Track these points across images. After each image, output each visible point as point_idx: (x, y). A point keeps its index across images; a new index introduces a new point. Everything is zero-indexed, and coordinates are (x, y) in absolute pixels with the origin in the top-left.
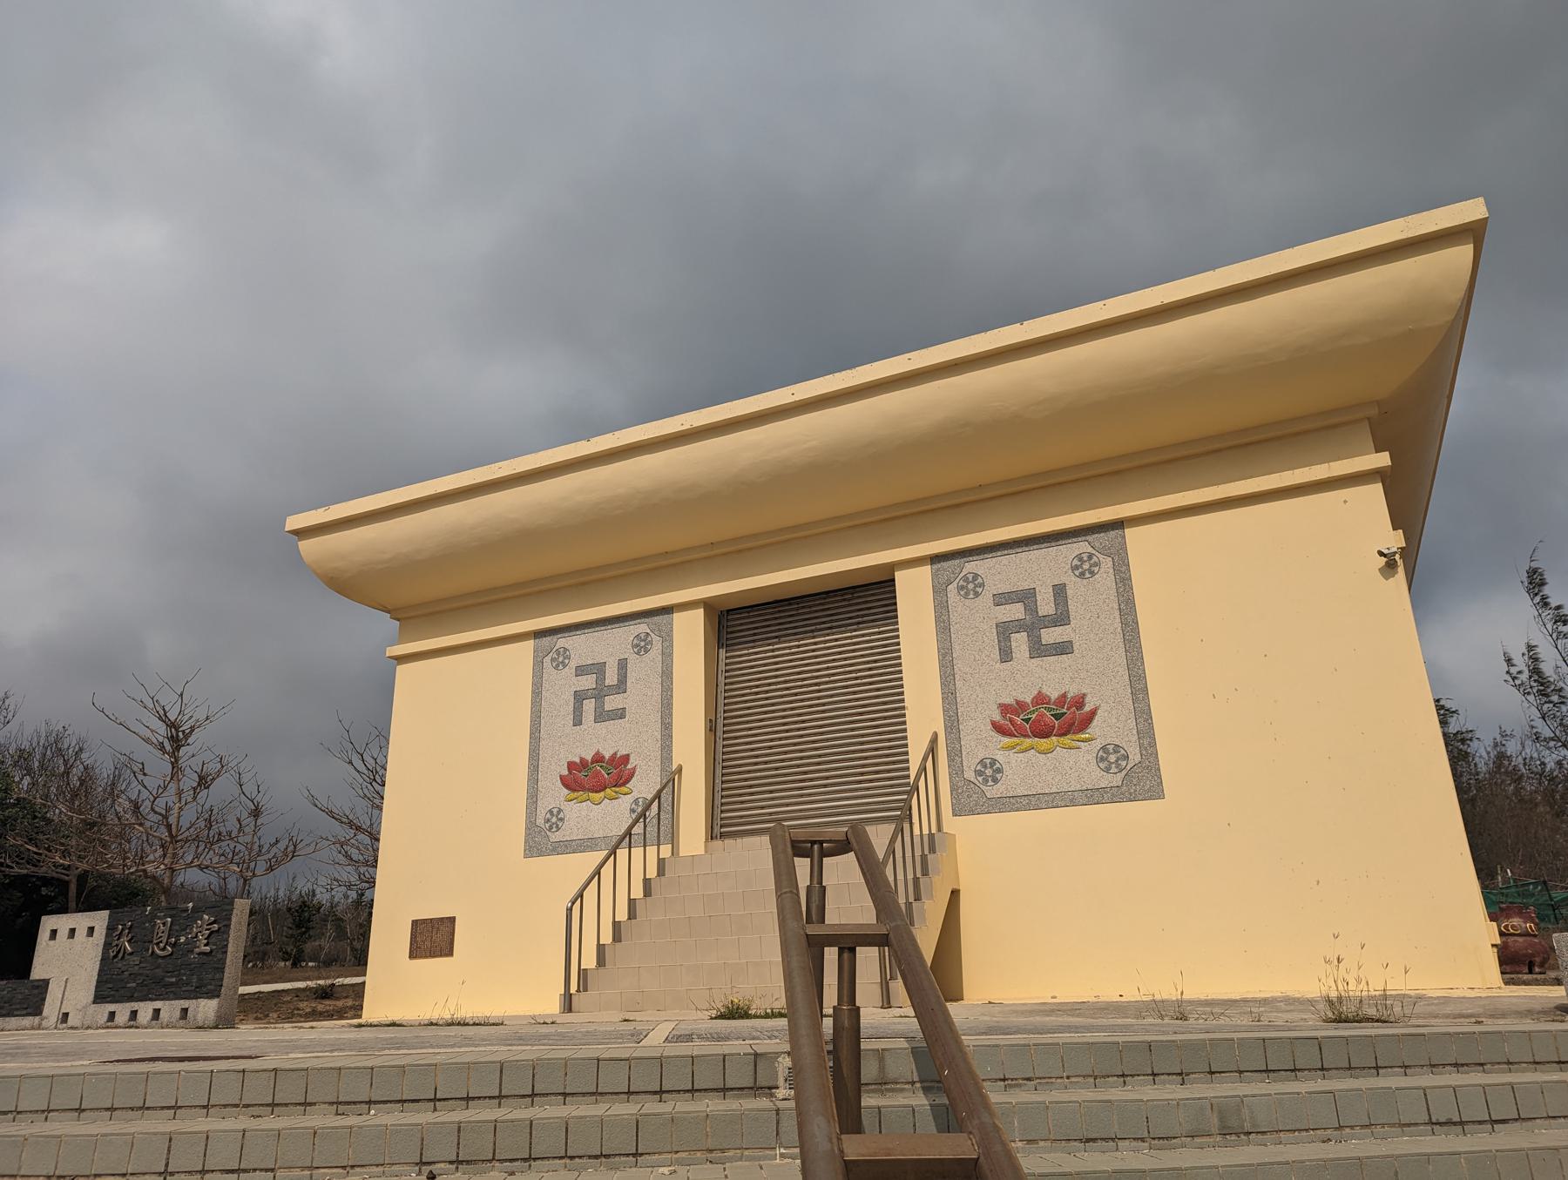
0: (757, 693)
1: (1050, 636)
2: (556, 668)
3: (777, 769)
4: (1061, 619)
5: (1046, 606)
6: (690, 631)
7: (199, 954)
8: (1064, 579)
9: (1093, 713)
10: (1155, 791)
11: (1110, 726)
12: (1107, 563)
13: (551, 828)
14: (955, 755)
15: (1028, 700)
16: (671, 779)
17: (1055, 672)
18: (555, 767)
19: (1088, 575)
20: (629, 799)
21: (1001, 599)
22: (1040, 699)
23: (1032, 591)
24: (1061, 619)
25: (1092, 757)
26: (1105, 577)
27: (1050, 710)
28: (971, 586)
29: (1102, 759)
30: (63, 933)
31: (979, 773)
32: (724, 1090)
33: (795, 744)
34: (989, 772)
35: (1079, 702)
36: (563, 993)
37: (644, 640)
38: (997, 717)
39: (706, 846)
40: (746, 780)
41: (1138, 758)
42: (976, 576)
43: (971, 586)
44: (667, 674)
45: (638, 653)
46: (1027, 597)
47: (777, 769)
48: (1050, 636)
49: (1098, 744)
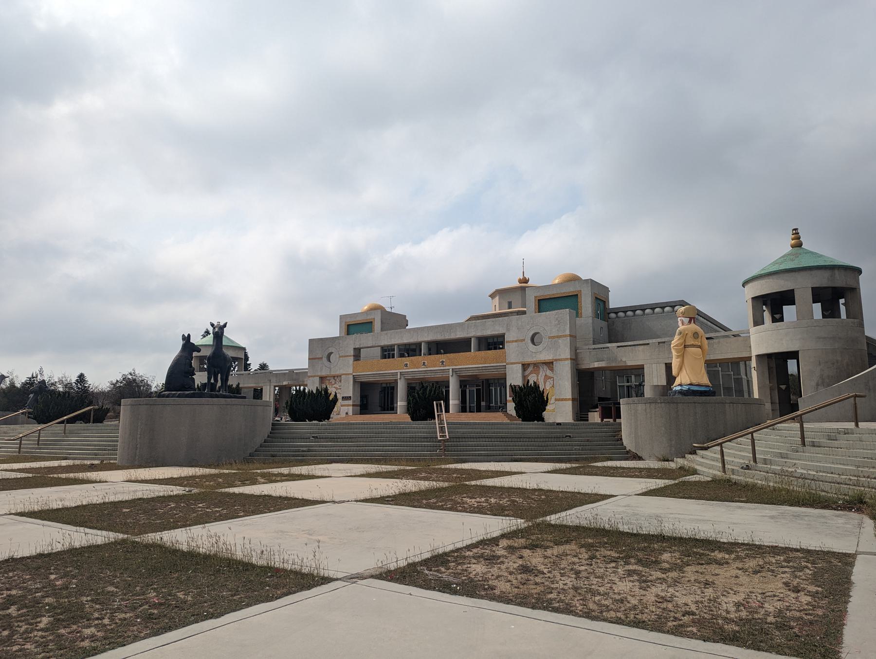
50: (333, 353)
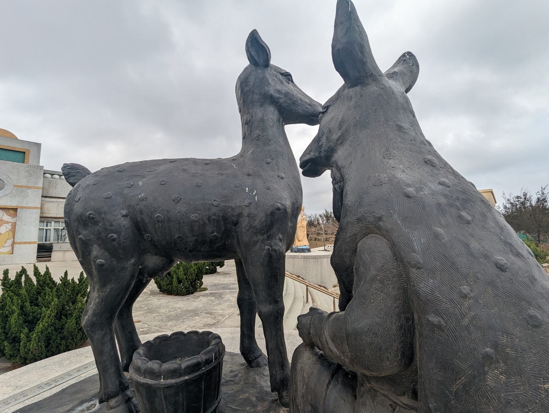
30: (330, 246)
50: (73, 278)
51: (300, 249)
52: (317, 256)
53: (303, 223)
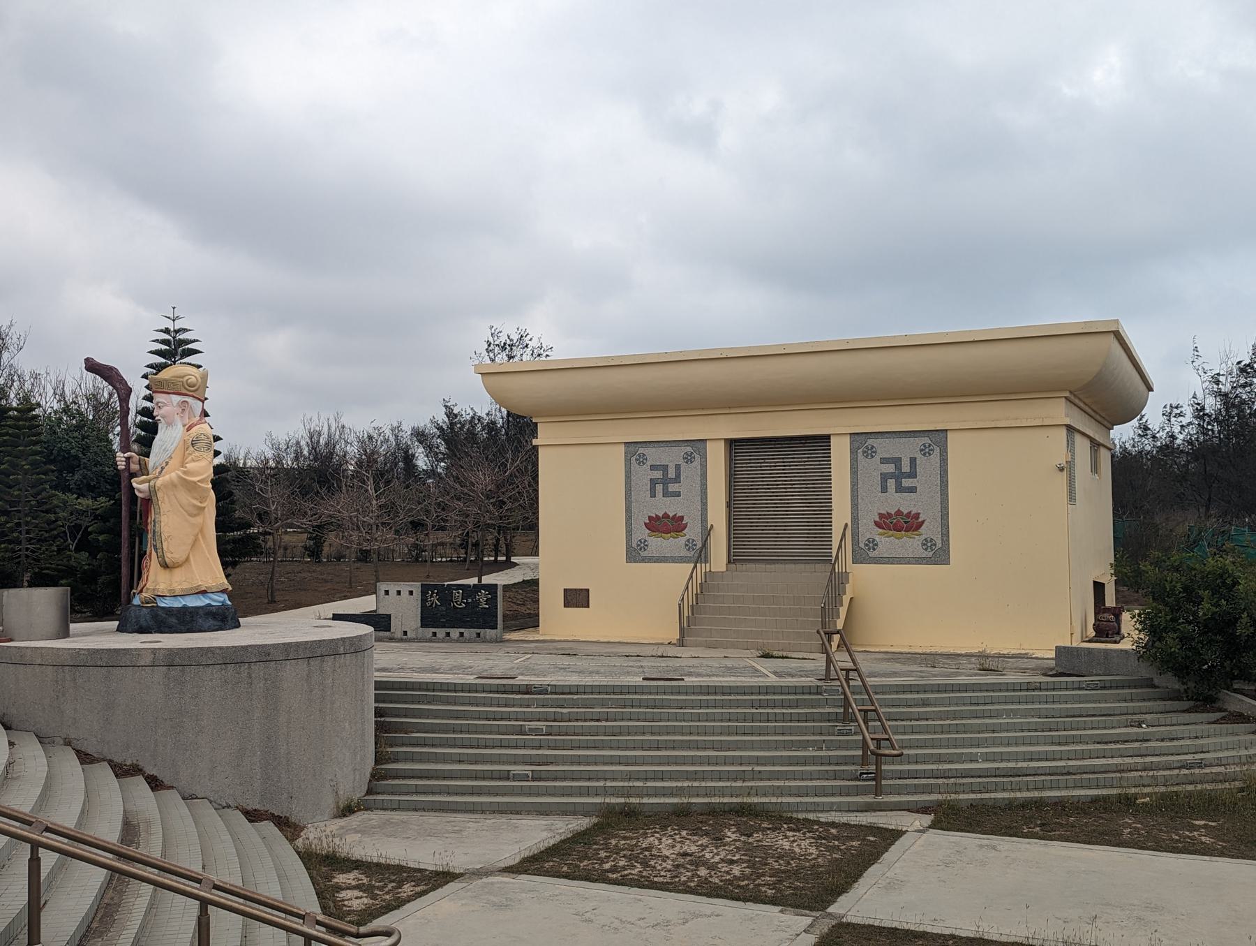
0: (751, 489)
1: (906, 483)
2: (639, 464)
3: (763, 530)
4: (912, 474)
5: (906, 468)
6: (717, 458)
7: (482, 608)
8: (916, 456)
9: (923, 522)
10: (946, 561)
11: (930, 529)
12: (937, 451)
13: (641, 549)
14: (855, 535)
15: (893, 513)
16: (707, 533)
17: (907, 500)
18: (641, 519)
19: (927, 455)
20: (685, 539)
21: (884, 461)
22: (899, 513)
23: (898, 491)
24: (912, 474)
25: (920, 543)
26: (935, 457)
27: (902, 519)
28: (869, 452)
29: (925, 544)
30: (393, 592)
31: (866, 545)
32: (810, 693)
33: (773, 519)
34: (871, 545)
35: (917, 516)
36: (678, 638)
37: (690, 456)
38: (877, 519)
39: (727, 567)
40: (746, 534)
41: (940, 545)
42: (873, 447)
43: (869, 452)
44: (704, 476)
45: (687, 462)
46: (897, 462)
47: (763, 530)
48: (906, 483)
49: (923, 537)
51: (169, 611)
52: (245, 648)
53: (190, 466)
